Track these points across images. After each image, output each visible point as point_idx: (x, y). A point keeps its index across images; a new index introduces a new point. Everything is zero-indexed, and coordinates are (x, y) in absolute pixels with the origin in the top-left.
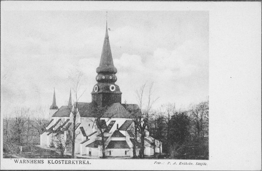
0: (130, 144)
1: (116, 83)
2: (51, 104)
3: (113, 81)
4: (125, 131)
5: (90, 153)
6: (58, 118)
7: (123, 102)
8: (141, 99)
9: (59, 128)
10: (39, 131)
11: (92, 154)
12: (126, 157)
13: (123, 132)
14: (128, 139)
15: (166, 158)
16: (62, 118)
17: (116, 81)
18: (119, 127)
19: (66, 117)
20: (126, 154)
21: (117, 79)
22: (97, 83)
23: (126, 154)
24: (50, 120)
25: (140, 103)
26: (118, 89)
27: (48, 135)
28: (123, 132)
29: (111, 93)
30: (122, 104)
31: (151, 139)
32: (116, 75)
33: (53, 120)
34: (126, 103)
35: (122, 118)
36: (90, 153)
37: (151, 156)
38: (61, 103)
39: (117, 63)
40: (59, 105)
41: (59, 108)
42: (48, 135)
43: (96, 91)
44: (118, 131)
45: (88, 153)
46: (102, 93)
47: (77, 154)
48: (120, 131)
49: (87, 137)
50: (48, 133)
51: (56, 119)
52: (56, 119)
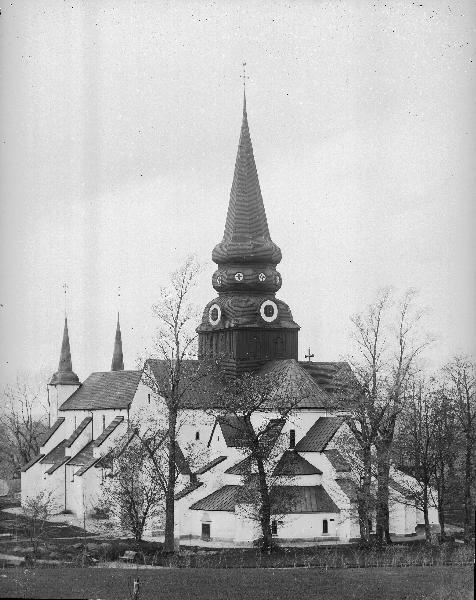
0: (341, 498)
1: (279, 295)
2: (54, 366)
3: (270, 289)
4: (318, 454)
5: (206, 529)
6: (82, 416)
7: (301, 358)
8: (373, 348)
9: (88, 447)
10: (177, 343)
11: (213, 534)
12: (325, 540)
13: (314, 458)
14: (328, 479)
15: (37, 485)
16: (98, 415)
17: (278, 287)
18: (298, 440)
19: (111, 412)
20: (325, 529)
21: (280, 279)
22: (215, 295)
23: (325, 529)
24: (54, 420)
25: (371, 360)
26: (285, 311)
27: (50, 473)
28: (314, 458)
29: (266, 329)
30: (301, 363)
31: (410, 482)
32: (279, 268)
33: (61, 421)
34: (313, 360)
35: (306, 411)
36: (206, 529)
37: (407, 536)
38: (91, 363)
39: (280, 231)
40: (82, 370)
41: (81, 381)
42: (50, 473)
43: (214, 323)
44: (296, 452)
45: (198, 531)
46: (237, 328)
47: (182, 538)
48: (302, 454)
49: (193, 477)
50: (49, 467)
51: (73, 419)
52: (73, 419)
